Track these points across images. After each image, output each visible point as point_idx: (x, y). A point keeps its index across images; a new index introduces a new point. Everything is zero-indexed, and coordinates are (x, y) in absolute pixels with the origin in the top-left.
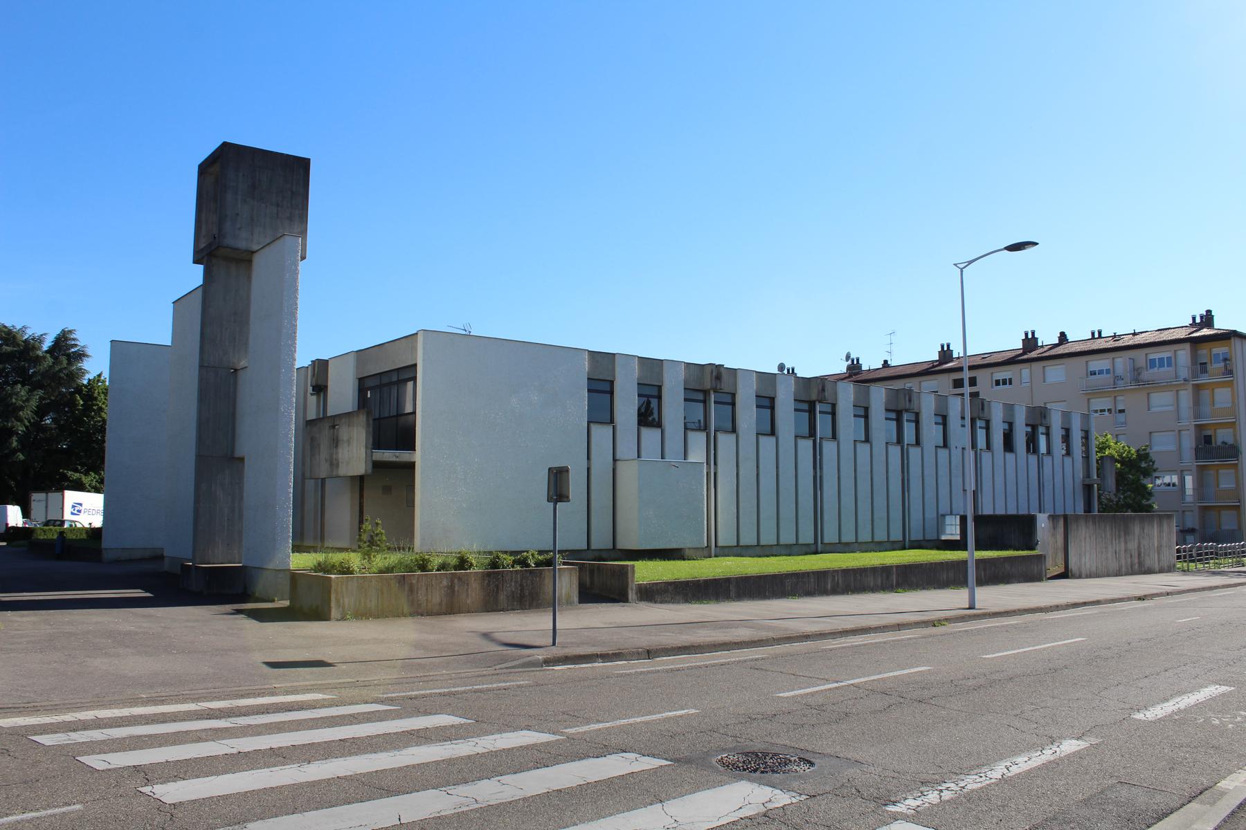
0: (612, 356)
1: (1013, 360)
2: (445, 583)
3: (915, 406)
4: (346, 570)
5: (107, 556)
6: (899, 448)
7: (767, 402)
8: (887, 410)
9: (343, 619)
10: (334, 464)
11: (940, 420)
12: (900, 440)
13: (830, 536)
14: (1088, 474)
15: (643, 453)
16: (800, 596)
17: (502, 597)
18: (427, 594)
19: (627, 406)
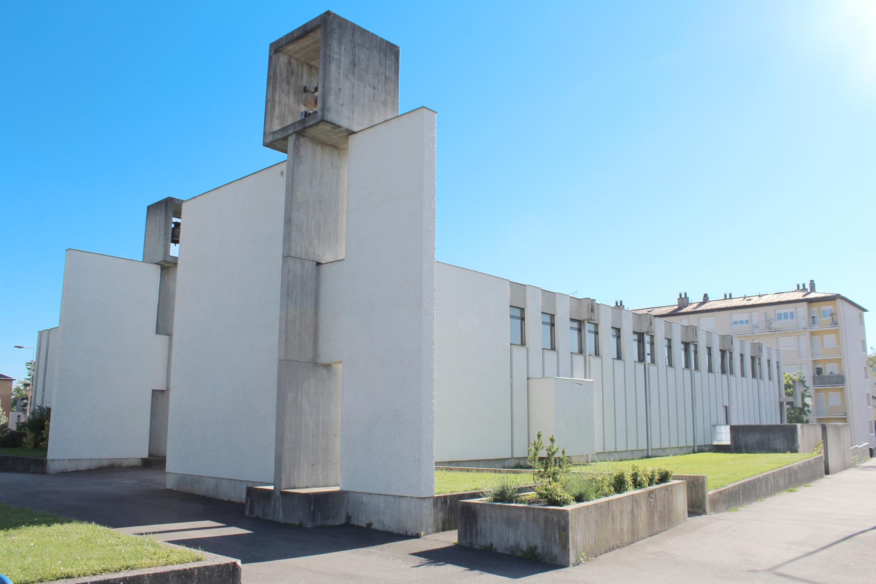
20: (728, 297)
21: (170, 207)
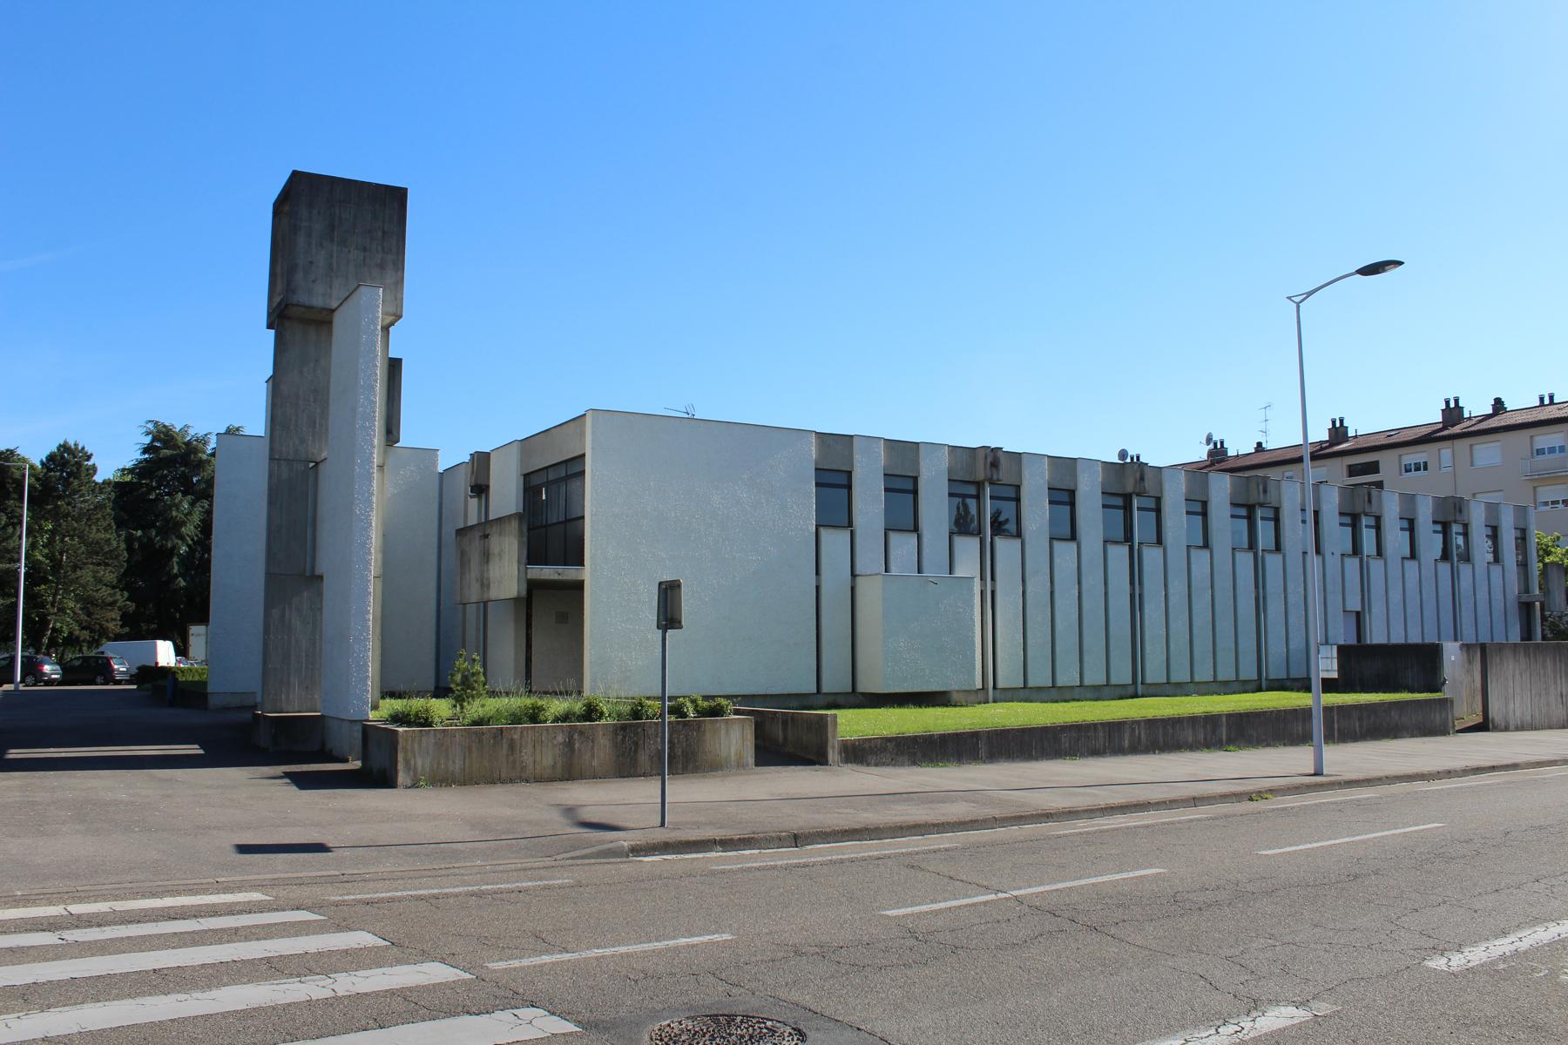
0: (849, 439)
1: (1428, 438)
2: (560, 738)
3: (1272, 498)
4: (423, 721)
5: (213, 701)
6: (1250, 555)
7: (1064, 497)
8: (1234, 505)
9: (415, 786)
10: (484, 584)
11: (1405, 524)
12: (1252, 545)
13: (1155, 673)
14: (1526, 589)
15: (893, 567)
16: (1082, 755)
17: (643, 758)
18: (534, 753)
19: (935, 508)
20: (1547, 401)
21: (669, 593)
